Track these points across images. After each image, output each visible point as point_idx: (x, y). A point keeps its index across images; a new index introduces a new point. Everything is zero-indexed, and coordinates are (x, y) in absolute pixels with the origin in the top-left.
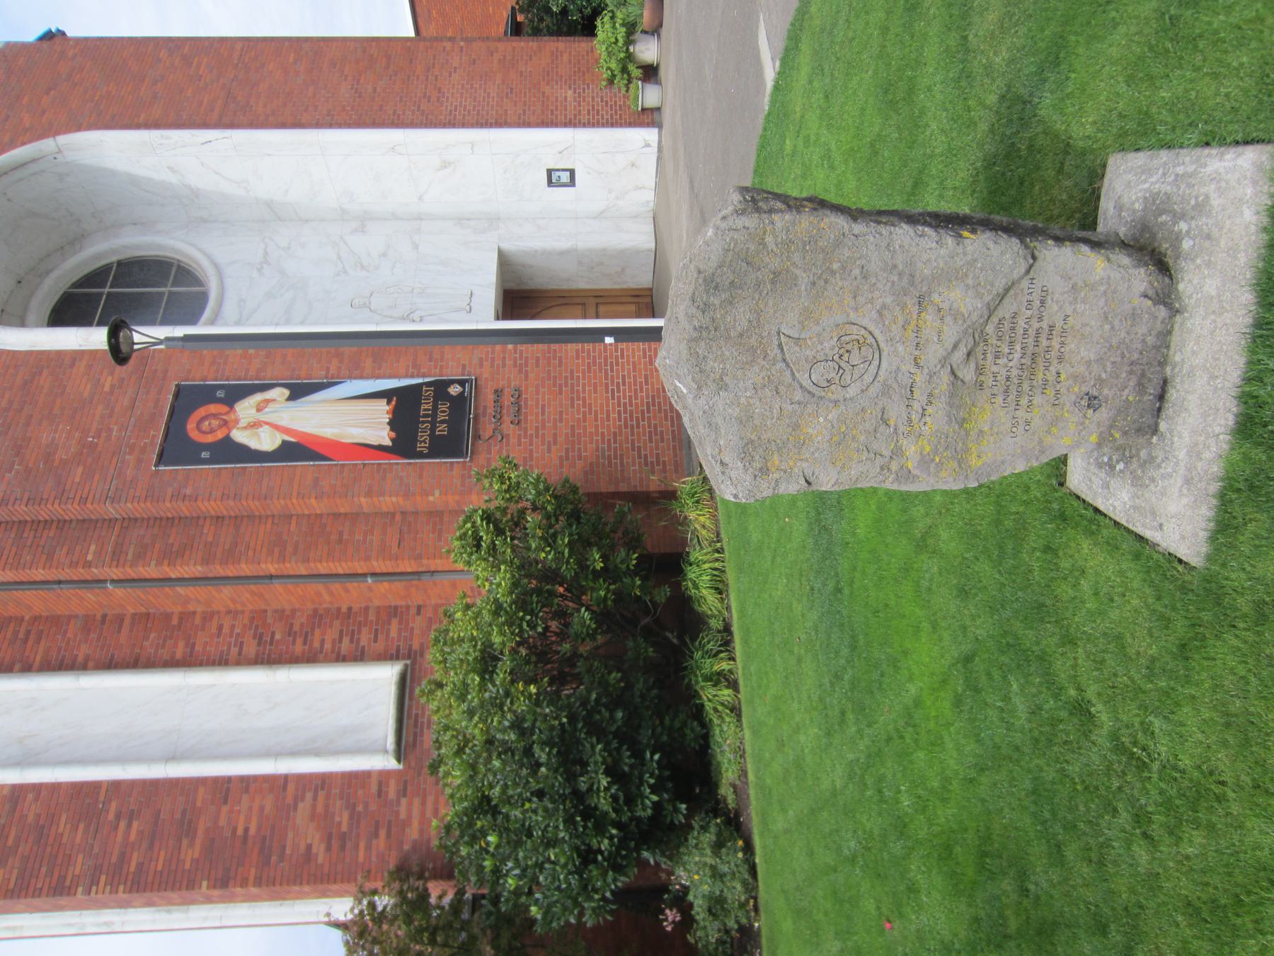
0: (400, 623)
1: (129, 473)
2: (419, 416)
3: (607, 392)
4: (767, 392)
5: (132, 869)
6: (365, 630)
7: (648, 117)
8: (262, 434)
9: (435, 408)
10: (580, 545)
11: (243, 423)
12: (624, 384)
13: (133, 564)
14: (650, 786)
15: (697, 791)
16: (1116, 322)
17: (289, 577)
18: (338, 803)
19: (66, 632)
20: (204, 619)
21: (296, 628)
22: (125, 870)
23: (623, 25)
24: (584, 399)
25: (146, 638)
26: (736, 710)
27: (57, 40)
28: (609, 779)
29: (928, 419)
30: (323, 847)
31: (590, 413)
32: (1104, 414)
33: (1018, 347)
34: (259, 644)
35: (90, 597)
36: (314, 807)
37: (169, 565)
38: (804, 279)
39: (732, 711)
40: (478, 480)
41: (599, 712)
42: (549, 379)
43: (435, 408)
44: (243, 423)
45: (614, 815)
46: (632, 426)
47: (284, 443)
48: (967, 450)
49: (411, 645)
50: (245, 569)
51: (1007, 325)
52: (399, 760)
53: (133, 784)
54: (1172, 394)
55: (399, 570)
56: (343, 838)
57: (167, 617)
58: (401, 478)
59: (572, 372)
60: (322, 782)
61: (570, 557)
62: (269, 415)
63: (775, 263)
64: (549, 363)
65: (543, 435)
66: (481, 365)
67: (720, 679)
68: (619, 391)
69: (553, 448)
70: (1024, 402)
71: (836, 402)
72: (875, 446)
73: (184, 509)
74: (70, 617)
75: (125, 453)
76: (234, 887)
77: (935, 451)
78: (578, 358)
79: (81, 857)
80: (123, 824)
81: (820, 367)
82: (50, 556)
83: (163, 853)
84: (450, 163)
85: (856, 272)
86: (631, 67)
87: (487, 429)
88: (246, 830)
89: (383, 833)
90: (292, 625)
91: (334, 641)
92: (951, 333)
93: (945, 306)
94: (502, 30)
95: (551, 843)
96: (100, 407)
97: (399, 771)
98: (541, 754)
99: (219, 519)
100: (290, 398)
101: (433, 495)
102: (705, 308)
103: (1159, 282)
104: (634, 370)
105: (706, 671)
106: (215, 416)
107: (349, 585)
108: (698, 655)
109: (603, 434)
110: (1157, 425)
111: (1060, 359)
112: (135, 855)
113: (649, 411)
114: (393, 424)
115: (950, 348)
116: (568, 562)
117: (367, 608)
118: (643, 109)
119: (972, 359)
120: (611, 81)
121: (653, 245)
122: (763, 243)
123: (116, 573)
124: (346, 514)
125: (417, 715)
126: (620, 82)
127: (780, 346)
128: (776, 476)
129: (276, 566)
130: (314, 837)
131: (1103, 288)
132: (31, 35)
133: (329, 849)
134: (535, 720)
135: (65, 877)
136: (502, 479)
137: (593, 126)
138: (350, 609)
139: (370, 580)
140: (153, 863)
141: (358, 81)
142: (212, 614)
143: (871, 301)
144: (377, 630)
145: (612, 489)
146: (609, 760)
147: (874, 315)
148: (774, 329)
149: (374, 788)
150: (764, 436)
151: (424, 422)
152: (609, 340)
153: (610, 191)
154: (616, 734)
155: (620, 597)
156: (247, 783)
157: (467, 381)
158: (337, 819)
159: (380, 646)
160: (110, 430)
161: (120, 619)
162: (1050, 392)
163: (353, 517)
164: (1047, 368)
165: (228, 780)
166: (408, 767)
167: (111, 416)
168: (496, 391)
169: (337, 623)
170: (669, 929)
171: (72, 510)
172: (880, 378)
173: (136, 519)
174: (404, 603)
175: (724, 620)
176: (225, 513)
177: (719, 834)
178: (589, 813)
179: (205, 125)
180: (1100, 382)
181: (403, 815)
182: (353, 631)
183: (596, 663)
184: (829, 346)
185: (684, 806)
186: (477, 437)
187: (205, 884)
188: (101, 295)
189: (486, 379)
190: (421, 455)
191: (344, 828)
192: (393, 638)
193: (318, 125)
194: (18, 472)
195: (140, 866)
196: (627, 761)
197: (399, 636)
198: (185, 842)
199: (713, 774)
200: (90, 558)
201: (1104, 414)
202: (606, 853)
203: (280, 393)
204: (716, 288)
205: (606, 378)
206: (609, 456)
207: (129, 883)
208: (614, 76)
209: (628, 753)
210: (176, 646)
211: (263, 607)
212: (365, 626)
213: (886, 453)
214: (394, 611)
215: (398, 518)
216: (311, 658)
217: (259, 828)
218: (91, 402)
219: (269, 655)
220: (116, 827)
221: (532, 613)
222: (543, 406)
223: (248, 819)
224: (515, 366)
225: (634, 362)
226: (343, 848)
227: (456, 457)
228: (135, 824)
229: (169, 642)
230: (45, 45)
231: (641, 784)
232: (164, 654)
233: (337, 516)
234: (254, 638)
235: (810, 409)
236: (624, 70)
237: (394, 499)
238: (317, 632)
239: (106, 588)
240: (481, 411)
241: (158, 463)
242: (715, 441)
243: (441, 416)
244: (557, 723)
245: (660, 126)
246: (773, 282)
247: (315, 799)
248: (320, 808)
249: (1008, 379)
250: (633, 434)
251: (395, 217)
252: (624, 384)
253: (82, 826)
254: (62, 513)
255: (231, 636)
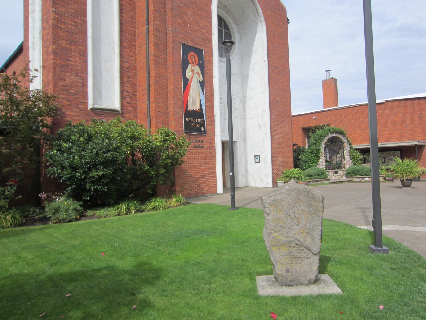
0: (132, 110)
1: (180, 35)
2: (195, 118)
3: (203, 173)
4: (288, 204)
5: (60, 25)
6: (130, 100)
7: (275, 184)
8: (190, 73)
9: (198, 123)
10: (166, 166)
11: (193, 68)
12: (205, 179)
13: (154, 34)
14: (97, 188)
15: (89, 203)
16: (304, 274)
17: (149, 79)
18: (78, 89)
19: (131, 12)
20: (134, 52)
21: (131, 79)
22: (59, 23)
23: (299, 176)
24: (201, 167)
25: (129, 34)
26: (119, 214)
27: (287, 22)
28: (101, 175)
29: (283, 237)
30: (65, 84)
31: (197, 169)
32: (285, 274)
33: (298, 254)
34: (126, 68)
35: (143, 20)
36: (77, 82)
37: (154, 44)
38: (310, 210)
39: (119, 213)
40: (183, 136)
41: (120, 172)
42: (206, 156)
43: (198, 123)
44: (193, 68)
45: (88, 177)
46: (193, 181)
47: (188, 79)
48: (276, 247)
49: (125, 113)
50: (152, 66)
51: (302, 251)
52: (91, 109)
53: (86, 28)
54: (291, 287)
55: (151, 111)
56: (67, 91)
57: (135, 41)
58: (179, 113)
59: (208, 163)
60: (85, 85)
61: (164, 163)
62: (195, 75)
63: (313, 204)
64: (210, 156)
65: (191, 155)
66: (209, 136)
67: (128, 209)
68: (203, 177)
69: (187, 158)
70: (287, 257)
71: (286, 218)
72: (277, 227)
73: (170, 50)
74: (135, 13)
75: (185, 34)
76: (53, 56)
77: (276, 240)
78: (212, 165)
79: (64, 10)
80: (74, 23)
81: (294, 214)
82: (156, 11)
83: (64, 35)
84: (260, 127)
85: (312, 220)
86: (288, 178)
87: (193, 138)
88: (71, 61)
89: (68, 103)
90: (132, 78)
91: (127, 90)
92: (301, 240)
93: (307, 238)
94: (294, 142)
95: (81, 157)
96: (197, 28)
97: (88, 109)
98: (109, 155)
99: (166, 59)
100: (200, 81)
101: (174, 122)
102: (304, 191)
103: (312, 282)
104: (209, 182)
105: (131, 205)
106: (195, 60)
107: (146, 95)
108: (135, 202)
109: (191, 172)
110: (283, 286)
111: (296, 263)
112: (64, 27)
113: (198, 186)
114: (193, 111)
115: (299, 240)
116: (162, 162)
117: (136, 100)
118: (277, 182)
119: (296, 245)
120: (283, 173)
121: (239, 186)
122: (317, 201)
123: (151, 29)
124: (167, 96)
125: (105, 115)
126: (284, 175)
127: (297, 206)
128: (270, 207)
129: (153, 75)
130: (68, 81)
131: (311, 270)
132: (288, 16)
133: (64, 86)
134: (119, 153)
135: (58, 5)
136: (184, 143)
137: (272, 168)
138: (136, 95)
139: (148, 102)
140: (61, 32)
141: (280, 102)
142: (135, 54)
143: (307, 223)
144: (130, 103)
145: (176, 175)
146: (106, 175)
147: (304, 224)
148: (300, 205)
149: (82, 101)
150: (278, 204)
151: (194, 120)
152: (231, 174)
153: (254, 173)
154: (113, 177)
155: (151, 178)
156: (85, 62)
157: (205, 132)
158: (73, 89)
159: (126, 104)
160: (191, 31)
161: (134, 27)
162: (289, 262)
163: (167, 98)
164: (294, 261)
165: (86, 56)
166: (89, 111)
167: (195, 31)
168: (202, 141)
169: (132, 91)
170: (40, 195)
171: (169, 18)
172: (292, 226)
173: (166, 36)
174: (138, 112)
175: (144, 210)
176: (168, 61)
177: (78, 210)
178: (90, 169)
179: (268, 60)
180: (292, 272)
181: (73, 109)
182: (130, 96)
183: (133, 171)
184: (298, 216)
185: (88, 199)
186: (190, 135)
187: (54, 47)
188: (222, 28)
189: (206, 138)
190: (185, 119)
191: (70, 91)
192: (127, 108)
193: (270, 91)
194: (180, 5)
195: (61, 28)
196: (106, 181)
197: (128, 110)
198: (68, 42)
199: (96, 208)
200: (156, 22)
201: (285, 274)
202: (75, 174)
203: (201, 78)
204: (308, 193)
205: (206, 173)
206: (185, 175)
207: (55, 24)
208: (285, 174)
209: (108, 181)
210: (126, 43)
211: (137, 70)
212: (131, 100)
213: (276, 230)
214: (135, 109)
215: (166, 112)
216: (122, 83)
217: (71, 65)
218: (198, 26)
219: (123, 71)
220: (73, 22)
221: (149, 152)
222: (198, 155)
223: (74, 61)
224: (209, 146)
225: (211, 181)
226: (64, 90)
227: (185, 128)
228: (74, 27)
229: (127, 41)
230: (286, 19)
231: (98, 185)
232: (124, 40)
233: (167, 94)
234: (128, 66)
235: (285, 213)
236: (287, 177)
237: (173, 111)
238: (130, 85)
239: (146, 26)
240: (197, 136)
241: (184, 44)
242: (276, 195)
243: (195, 125)
244: (119, 159)
245: (273, 187)
246: (309, 204)
247: (80, 82)
248: (76, 84)
249: (292, 253)
250: (191, 181)
251: (244, 111)
252: (205, 179)
253: (74, 11)
254: (169, 16)
255: (129, 59)
